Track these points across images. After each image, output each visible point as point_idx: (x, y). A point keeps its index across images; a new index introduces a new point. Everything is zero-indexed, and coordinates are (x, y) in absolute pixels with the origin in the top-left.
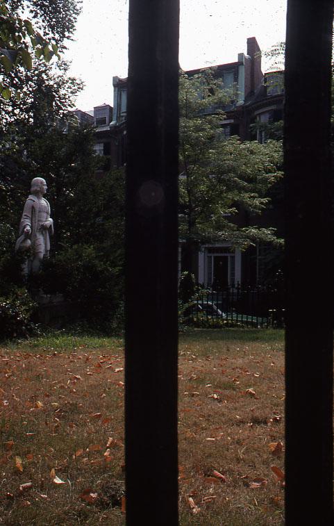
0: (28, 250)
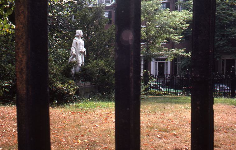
0: (74, 63)
